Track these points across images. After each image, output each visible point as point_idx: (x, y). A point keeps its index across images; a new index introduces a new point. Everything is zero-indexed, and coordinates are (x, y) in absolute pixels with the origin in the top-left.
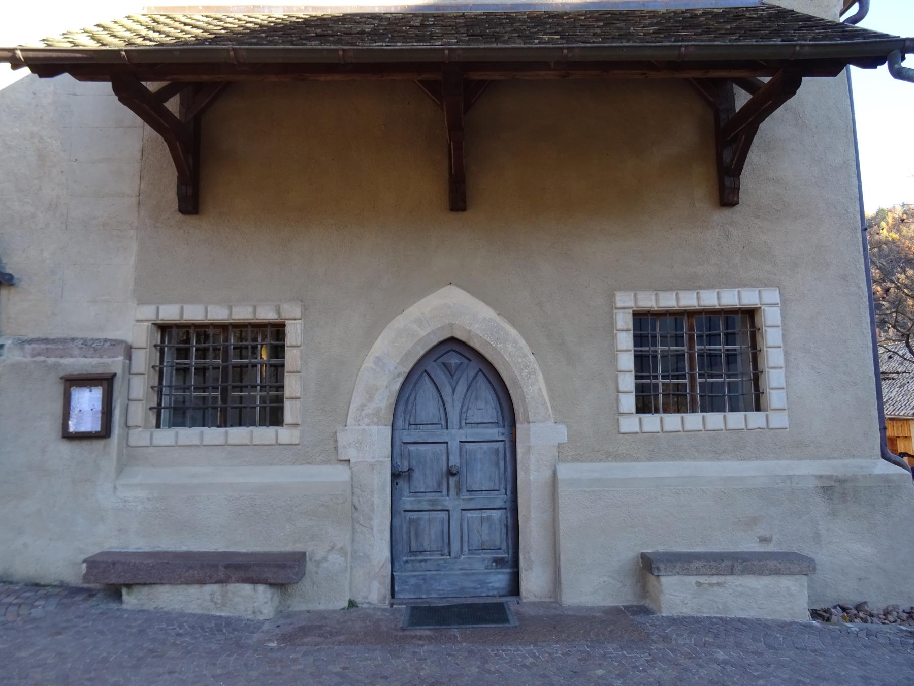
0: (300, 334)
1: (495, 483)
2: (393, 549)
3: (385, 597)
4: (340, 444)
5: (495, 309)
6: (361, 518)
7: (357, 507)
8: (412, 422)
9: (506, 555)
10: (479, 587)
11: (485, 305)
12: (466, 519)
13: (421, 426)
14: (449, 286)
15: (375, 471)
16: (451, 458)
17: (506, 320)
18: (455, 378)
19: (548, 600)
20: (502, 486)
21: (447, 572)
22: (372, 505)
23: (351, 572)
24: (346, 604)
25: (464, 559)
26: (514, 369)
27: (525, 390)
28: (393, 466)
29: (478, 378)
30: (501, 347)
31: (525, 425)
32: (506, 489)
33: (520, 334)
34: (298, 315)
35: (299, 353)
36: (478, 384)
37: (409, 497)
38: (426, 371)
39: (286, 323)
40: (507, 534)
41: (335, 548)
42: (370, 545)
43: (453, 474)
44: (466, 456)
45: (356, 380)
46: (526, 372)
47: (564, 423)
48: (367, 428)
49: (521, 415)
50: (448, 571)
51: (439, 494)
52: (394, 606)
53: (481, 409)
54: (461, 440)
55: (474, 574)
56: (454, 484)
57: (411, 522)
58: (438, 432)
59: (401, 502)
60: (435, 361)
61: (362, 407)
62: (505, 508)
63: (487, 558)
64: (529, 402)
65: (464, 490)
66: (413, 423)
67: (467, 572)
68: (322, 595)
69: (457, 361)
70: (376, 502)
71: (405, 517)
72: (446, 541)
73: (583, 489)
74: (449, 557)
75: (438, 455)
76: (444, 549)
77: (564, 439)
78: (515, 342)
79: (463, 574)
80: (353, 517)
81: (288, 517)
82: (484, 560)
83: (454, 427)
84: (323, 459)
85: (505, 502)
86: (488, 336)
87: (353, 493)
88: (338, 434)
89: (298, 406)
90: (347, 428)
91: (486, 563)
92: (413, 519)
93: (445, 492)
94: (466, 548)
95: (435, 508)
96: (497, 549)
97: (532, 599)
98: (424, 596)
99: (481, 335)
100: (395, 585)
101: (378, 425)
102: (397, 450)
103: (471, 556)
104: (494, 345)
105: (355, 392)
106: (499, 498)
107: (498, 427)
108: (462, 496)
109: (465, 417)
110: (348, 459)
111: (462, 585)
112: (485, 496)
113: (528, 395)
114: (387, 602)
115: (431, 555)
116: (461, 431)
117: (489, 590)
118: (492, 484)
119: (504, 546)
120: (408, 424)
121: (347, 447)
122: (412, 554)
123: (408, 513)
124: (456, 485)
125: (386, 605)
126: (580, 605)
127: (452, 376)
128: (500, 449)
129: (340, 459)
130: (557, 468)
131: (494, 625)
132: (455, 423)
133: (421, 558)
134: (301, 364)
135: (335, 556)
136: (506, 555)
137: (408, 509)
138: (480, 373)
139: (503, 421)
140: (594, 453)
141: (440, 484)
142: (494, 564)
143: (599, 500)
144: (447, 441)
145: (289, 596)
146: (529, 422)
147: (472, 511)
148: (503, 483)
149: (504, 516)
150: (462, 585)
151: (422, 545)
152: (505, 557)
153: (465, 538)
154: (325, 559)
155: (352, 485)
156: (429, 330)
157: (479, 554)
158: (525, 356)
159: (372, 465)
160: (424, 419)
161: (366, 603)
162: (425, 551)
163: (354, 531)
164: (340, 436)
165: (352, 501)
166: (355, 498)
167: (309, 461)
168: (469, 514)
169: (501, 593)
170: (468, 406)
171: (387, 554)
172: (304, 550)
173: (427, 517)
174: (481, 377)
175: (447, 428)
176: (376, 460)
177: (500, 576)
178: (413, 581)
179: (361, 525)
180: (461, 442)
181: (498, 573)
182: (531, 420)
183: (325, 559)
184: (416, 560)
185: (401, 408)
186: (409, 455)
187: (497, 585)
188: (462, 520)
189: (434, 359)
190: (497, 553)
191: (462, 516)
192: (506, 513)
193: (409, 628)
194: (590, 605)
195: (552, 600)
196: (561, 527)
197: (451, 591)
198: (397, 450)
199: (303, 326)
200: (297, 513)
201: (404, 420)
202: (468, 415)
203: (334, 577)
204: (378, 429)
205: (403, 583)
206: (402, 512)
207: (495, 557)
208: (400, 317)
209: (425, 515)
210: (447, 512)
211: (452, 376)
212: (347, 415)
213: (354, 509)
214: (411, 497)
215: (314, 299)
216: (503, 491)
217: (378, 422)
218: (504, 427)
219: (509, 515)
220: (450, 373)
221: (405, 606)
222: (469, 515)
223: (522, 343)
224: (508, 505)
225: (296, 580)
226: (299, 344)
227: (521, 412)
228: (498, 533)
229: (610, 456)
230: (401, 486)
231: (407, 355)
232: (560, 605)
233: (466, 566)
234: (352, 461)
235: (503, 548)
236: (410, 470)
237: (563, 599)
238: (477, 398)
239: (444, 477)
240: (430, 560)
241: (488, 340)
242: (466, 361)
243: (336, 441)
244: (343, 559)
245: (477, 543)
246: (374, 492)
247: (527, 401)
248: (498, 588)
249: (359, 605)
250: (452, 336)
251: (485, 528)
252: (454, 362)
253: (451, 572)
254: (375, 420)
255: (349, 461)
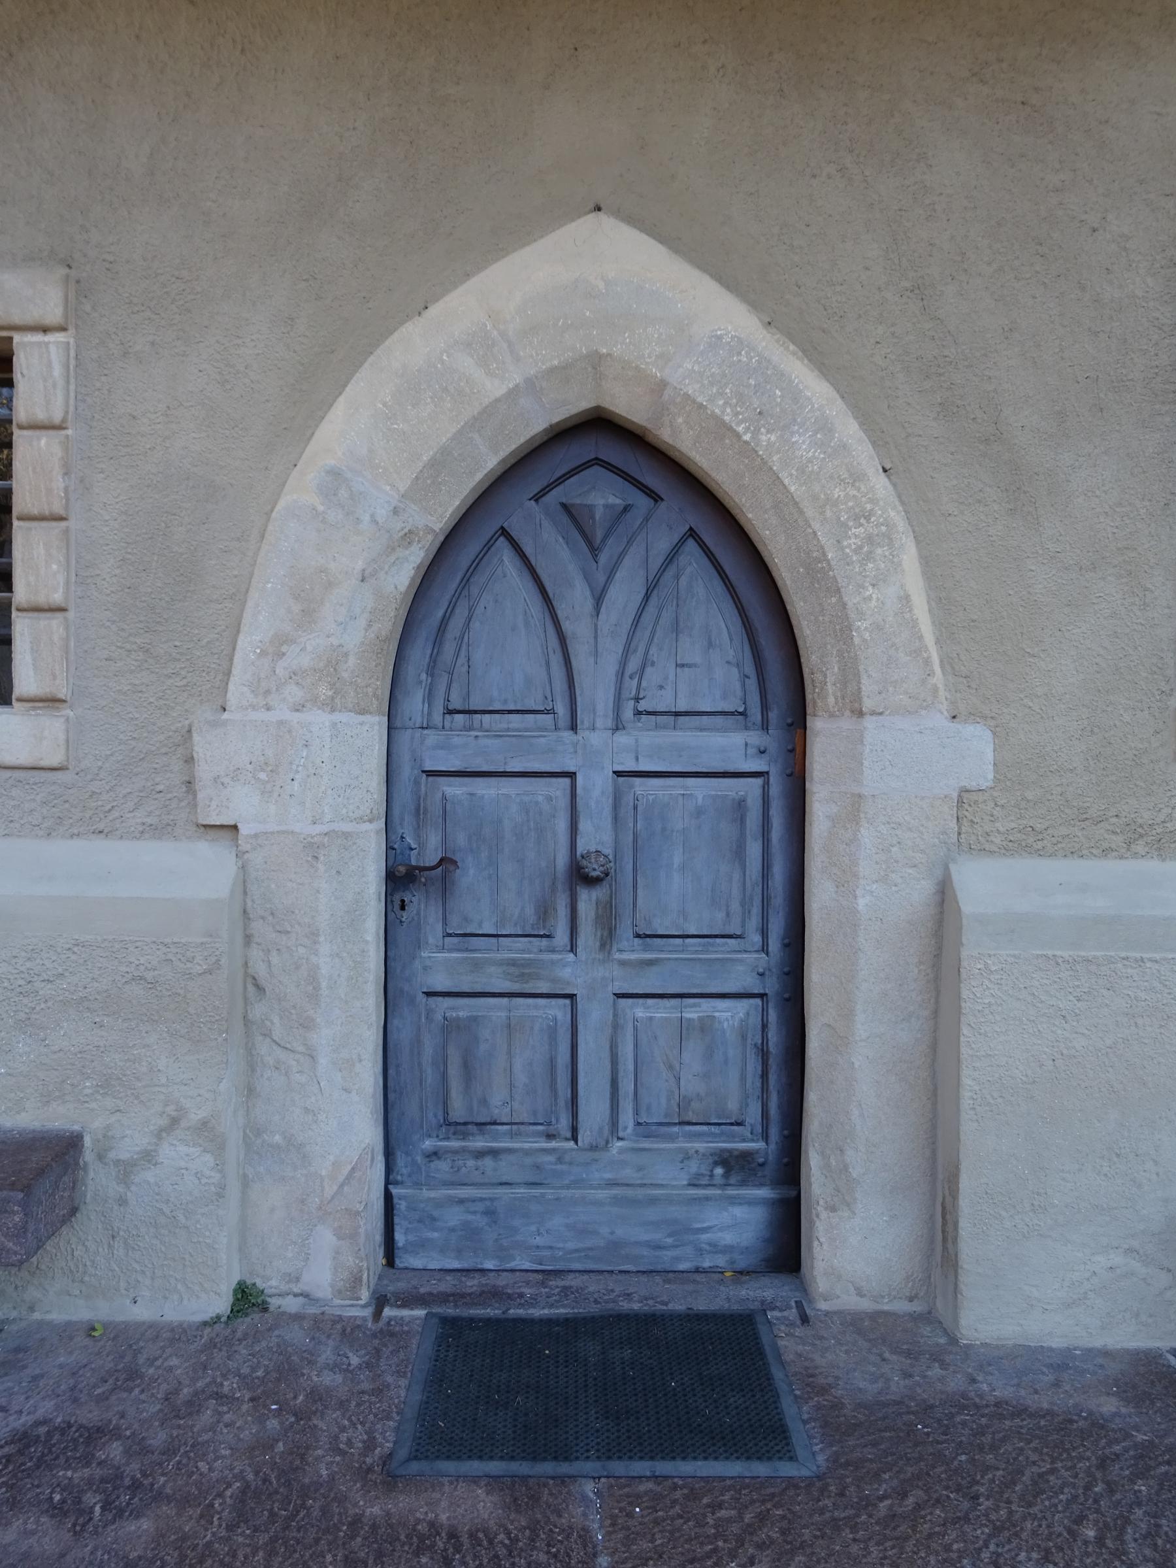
0: (61, 383)
1: (728, 915)
2: (394, 1114)
3: (357, 1281)
4: (204, 771)
5: (754, 305)
6: (276, 1020)
7: (263, 983)
8: (456, 703)
9: (759, 1145)
10: (670, 1240)
11: (723, 290)
12: (631, 1025)
13: (487, 718)
14: (592, 217)
15: (321, 867)
16: (584, 825)
17: (792, 347)
18: (603, 558)
19: (901, 1306)
20: (754, 922)
21: (564, 1193)
22: (313, 978)
23: (244, 1200)
24: (221, 1304)
25: (622, 1151)
26: (816, 525)
27: (851, 600)
28: (390, 848)
29: (683, 559)
30: (770, 444)
31: (846, 723)
32: (764, 932)
33: (843, 397)
34: (53, 313)
35: (57, 451)
36: (683, 581)
37: (443, 949)
38: (504, 532)
39: (15, 341)
40: (764, 1076)
41: (184, 1124)
42: (307, 1110)
43: (591, 881)
44: (635, 821)
45: (259, 549)
46: (856, 536)
47: (985, 718)
48: (296, 717)
49: (830, 688)
50: (568, 1187)
51: (544, 942)
52: (388, 1312)
53: (689, 666)
54: (620, 768)
55: (653, 1201)
56: (592, 914)
57: (450, 1027)
58: (542, 740)
59: (417, 964)
60: (537, 498)
61: (277, 647)
62: (762, 996)
63: (697, 1152)
64: (865, 640)
65: (625, 931)
66: (459, 707)
67: (630, 1192)
68: (143, 1272)
69: (612, 500)
70: (324, 971)
71: (429, 1013)
72: (564, 1092)
73: (1050, 953)
74: (572, 1143)
75: (541, 814)
76: (557, 1120)
77: (985, 776)
78: (825, 427)
79: (617, 1201)
80: (250, 1016)
81: (22, 1016)
82: (687, 1157)
83: (599, 724)
84: (149, 821)
85: (761, 975)
86: (726, 403)
87: (248, 939)
88: (196, 737)
89: (56, 638)
90: (226, 716)
91: (694, 1166)
92: (458, 1019)
93: (561, 936)
94: (627, 1119)
95: (528, 988)
96: (732, 1124)
97: (850, 1301)
98: (489, 1265)
99: (699, 400)
100: (397, 1228)
101: (333, 710)
102: (404, 795)
103: (646, 1144)
104: (747, 437)
105: (254, 595)
106: (741, 961)
107: (746, 728)
108: (620, 951)
109: (634, 692)
110: (232, 823)
111: (612, 1233)
112: (696, 952)
113: (861, 615)
114: (365, 1295)
115: (512, 1135)
116: (622, 738)
117: (700, 1252)
118: (720, 916)
119: (753, 1114)
120: (441, 710)
121: (226, 780)
122: (452, 1129)
123: (440, 999)
124: (597, 917)
125: (359, 1310)
126: (1021, 1342)
127: (594, 551)
128: (749, 801)
129: (205, 823)
130: (955, 876)
131: (734, 1468)
132: (600, 708)
133: (479, 1143)
134: (66, 489)
135: (183, 1149)
136: (759, 1145)
137: (439, 988)
138: (691, 544)
139: (765, 707)
140: (1083, 825)
141: (545, 911)
142: (719, 1171)
143: (1105, 992)
144: (572, 769)
145: (33, 1274)
146: (861, 714)
147: (650, 1001)
148: (756, 910)
149: (755, 1020)
150: (612, 1233)
151: (484, 1102)
152: (757, 1151)
153: (627, 1086)
154: (148, 1157)
155: (245, 911)
156: (516, 377)
157: (672, 1138)
158: (857, 477)
159: (311, 844)
160: (495, 694)
161: (296, 1295)
162: (495, 1123)
163: (252, 1065)
164: (201, 745)
165: (246, 964)
166: (255, 953)
167: (101, 826)
168: (639, 1010)
169: (742, 1264)
170: (646, 653)
171: (369, 1134)
172: (76, 1127)
173: (504, 1014)
174: (692, 561)
175: (574, 727)
176: (325, 828)
177: (739, 1212)
178: (454, 1217)
179: (274, 1041)
180: (618, 774)
181: (733, 1201)
182: (868, 704)
183: (148, 1157)
184: (464, 1150)
185: (419, 654)
186: (445, 811)
187: (728, 1238)
188: (616, 1027)
189: (535, 489)
190: (732, 1137)
191: (615, 1015)
192: (764, 1011)
193: (415, 1467)
194: (1057, 1343)
195: (917, 1307)
196: (966, 1081)
197: (577, 1251)
198: (404, 795)
199: (72, 354)
200: (50, 1004)
201: (430, 696)
202: (644, 684)
203: (181, 1218)
204: (334, 725)
205: (420, 1221)
206: (421, 998)
207: (723, 1150)
208: (412, 330)
209: (496, 1010)
210: (568, 1002)
211: (594, 551)
212: (228, 673)
213: (251, 989)
214: (450, 951)
215: (111, 258)
216: (757, 938)
217: (333, 698)
218: (765, 726)
219: (773, 1016)
220: (589, 542)
221: (420, 1313)
222: (640, 1013)
223: (849, 429)
224: (772, 986)
225: (16, 1253)
226: (57, 417)
227: (830, 679)
228: (734, 1075)
229: (1141, 836)
230: (418, 914)
231: (439, 464)
232: (954, 1341)
233: (628, 1174)
234: (244, 830)
235: (749, 1120)
236: (447, 862)
237: (963, 1322)
238: (676, 629)
239: (560, 887)
240: (510, 1151)
241: (727, 418)
242: (642, 502)
243: (190, 760)
244: (209, 1159)
245: (664, 1101)
246: (318, 935)
247: (857, 641)
248: (728, 1249)
249: (274, 1302)
250: (598, 408)
251: (692, 1058)
252: (601, 502)
253: (578, 1193)
254: (324, 691)
255: (235, 827)
